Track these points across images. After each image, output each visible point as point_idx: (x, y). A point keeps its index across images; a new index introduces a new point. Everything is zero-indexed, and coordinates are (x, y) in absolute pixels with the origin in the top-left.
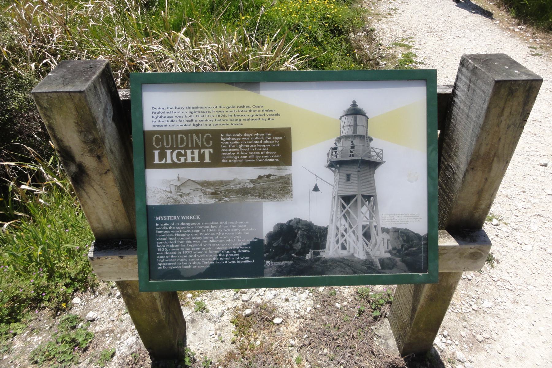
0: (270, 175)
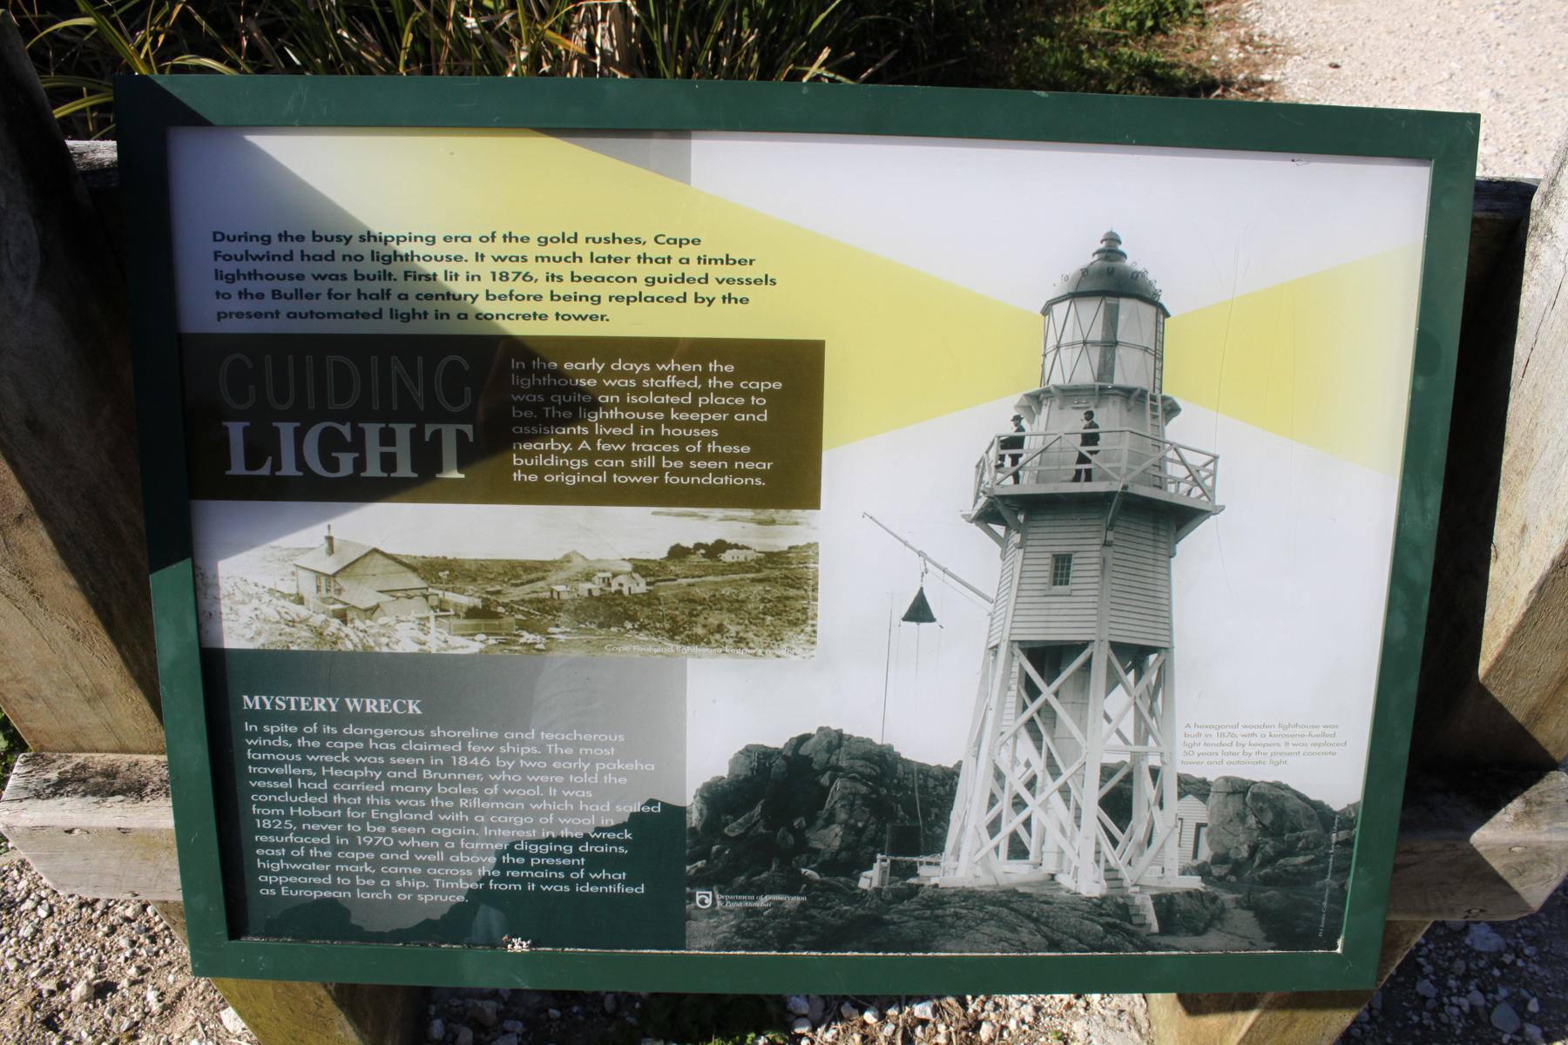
0: (721, 546)
